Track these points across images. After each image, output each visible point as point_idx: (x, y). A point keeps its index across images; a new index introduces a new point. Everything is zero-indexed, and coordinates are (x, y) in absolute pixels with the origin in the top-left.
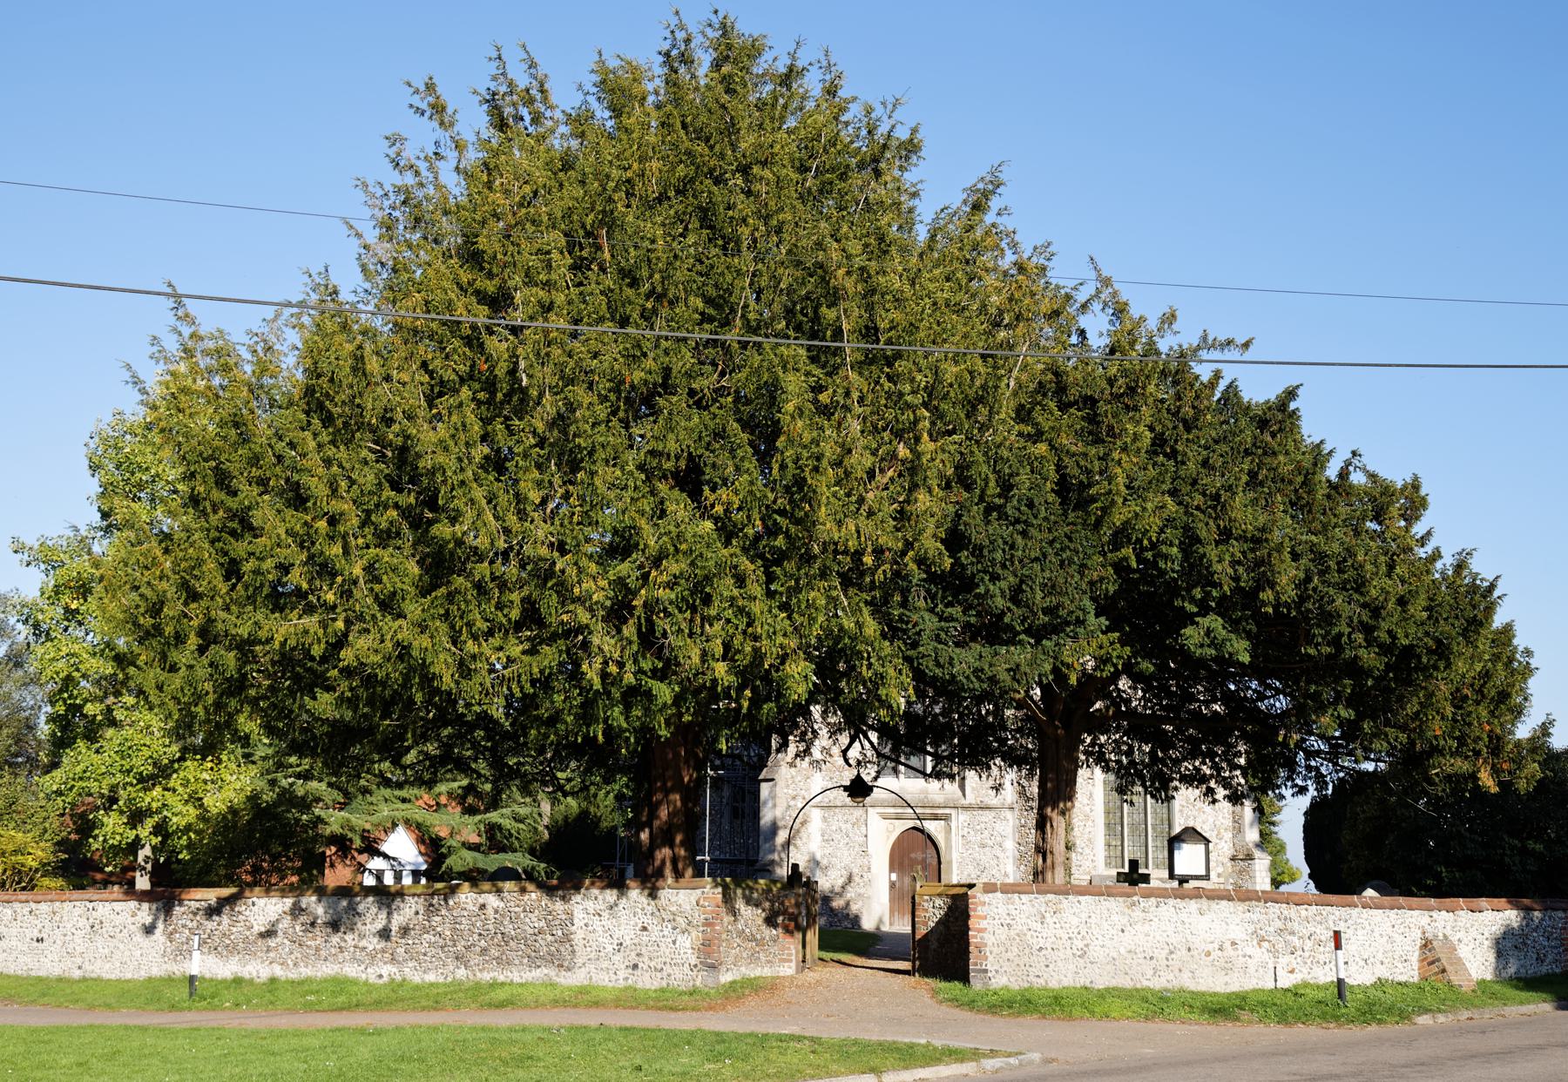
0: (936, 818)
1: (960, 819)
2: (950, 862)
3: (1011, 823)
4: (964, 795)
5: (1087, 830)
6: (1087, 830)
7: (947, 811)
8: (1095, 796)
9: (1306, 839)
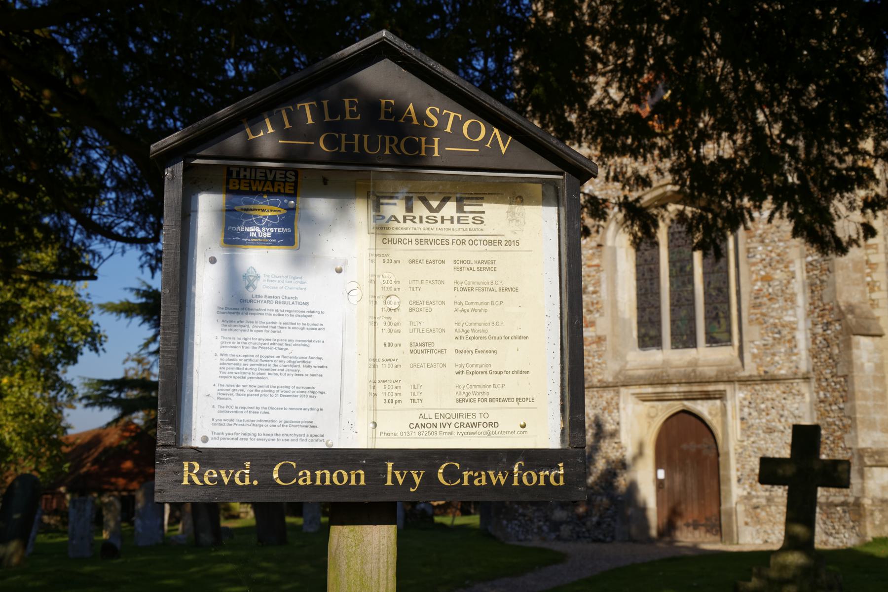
0: (707, 396)
1: (737, 396)
2: (727, 454)
3: (807, 398)
4: (743, 365)
7: (721, 387)
9: (375, 524)
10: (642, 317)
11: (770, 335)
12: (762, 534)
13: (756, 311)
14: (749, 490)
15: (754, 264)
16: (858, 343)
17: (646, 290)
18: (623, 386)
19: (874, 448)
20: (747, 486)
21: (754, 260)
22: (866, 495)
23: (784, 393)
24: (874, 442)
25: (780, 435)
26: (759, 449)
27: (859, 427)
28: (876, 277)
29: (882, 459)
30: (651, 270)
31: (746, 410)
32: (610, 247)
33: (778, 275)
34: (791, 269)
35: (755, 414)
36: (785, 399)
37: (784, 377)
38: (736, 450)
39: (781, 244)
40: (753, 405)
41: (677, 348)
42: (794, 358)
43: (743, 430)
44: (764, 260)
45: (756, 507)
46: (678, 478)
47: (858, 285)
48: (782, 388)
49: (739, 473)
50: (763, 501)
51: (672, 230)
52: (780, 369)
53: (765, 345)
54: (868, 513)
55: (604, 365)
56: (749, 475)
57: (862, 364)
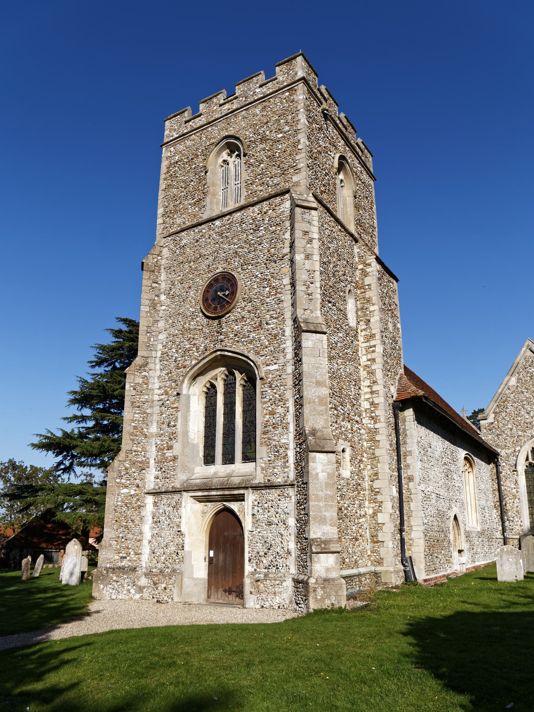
1: (251, 497)
5: (516, 505)
6: (516, 505)
7: (241, 492)
8: (519, 482)
10: (207, 442)
11: (273, 453)
12: (260, 601)
13: (265, 436)
14: (255, 567)
15: (265, 403)
16: (315, 458)
17: (210, 424)
18: (184, 491)
19: (323, 538)
20: (254, 565)
21: (265, 400)
22: (313, 575)
23: (279, 496)
24: (324, 534)
25: (275, 526)
26: (263, 537)
27: (312, 522)
28: (378, 413)
29: (327, 546)
30: (213, 409)
31: (256, 508)
32: (185, 395)
33: (280, 410)
34: (287, 405)
35: (261, 511)
36: (279, 500)
37: (279, 484)
38: (249, 538)
39: (282, 388)
40: (260, 505)
41: (226, 464)
42: (286, 470)
43: (253, 522)
44: (271, 399)
45: (258, 581)
46: (221, 557)
47: (322, 414)
48: (278, 491)
49: (250, 555)
50: (262, 576)
51: (226, 383)
52: (278, 478)
53: (269, 461)
54: (311, 590)
55: (176, 476)
56: (255, 557)
57: (317, 474)
